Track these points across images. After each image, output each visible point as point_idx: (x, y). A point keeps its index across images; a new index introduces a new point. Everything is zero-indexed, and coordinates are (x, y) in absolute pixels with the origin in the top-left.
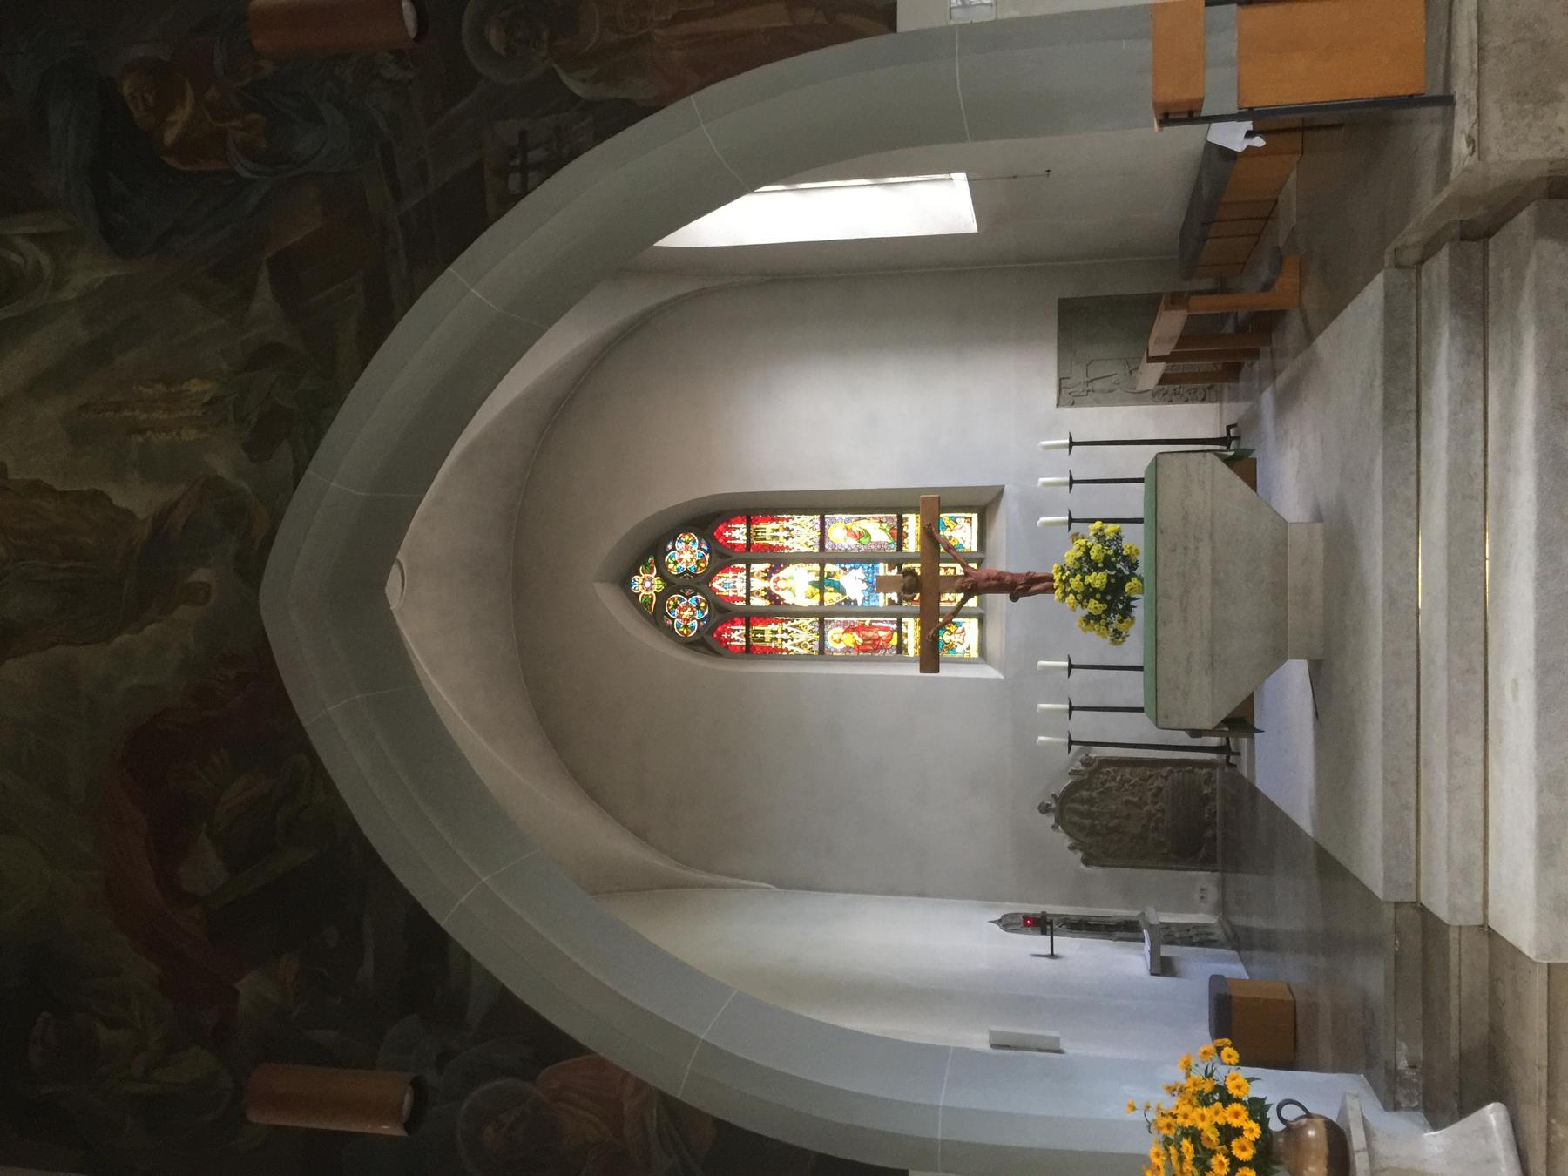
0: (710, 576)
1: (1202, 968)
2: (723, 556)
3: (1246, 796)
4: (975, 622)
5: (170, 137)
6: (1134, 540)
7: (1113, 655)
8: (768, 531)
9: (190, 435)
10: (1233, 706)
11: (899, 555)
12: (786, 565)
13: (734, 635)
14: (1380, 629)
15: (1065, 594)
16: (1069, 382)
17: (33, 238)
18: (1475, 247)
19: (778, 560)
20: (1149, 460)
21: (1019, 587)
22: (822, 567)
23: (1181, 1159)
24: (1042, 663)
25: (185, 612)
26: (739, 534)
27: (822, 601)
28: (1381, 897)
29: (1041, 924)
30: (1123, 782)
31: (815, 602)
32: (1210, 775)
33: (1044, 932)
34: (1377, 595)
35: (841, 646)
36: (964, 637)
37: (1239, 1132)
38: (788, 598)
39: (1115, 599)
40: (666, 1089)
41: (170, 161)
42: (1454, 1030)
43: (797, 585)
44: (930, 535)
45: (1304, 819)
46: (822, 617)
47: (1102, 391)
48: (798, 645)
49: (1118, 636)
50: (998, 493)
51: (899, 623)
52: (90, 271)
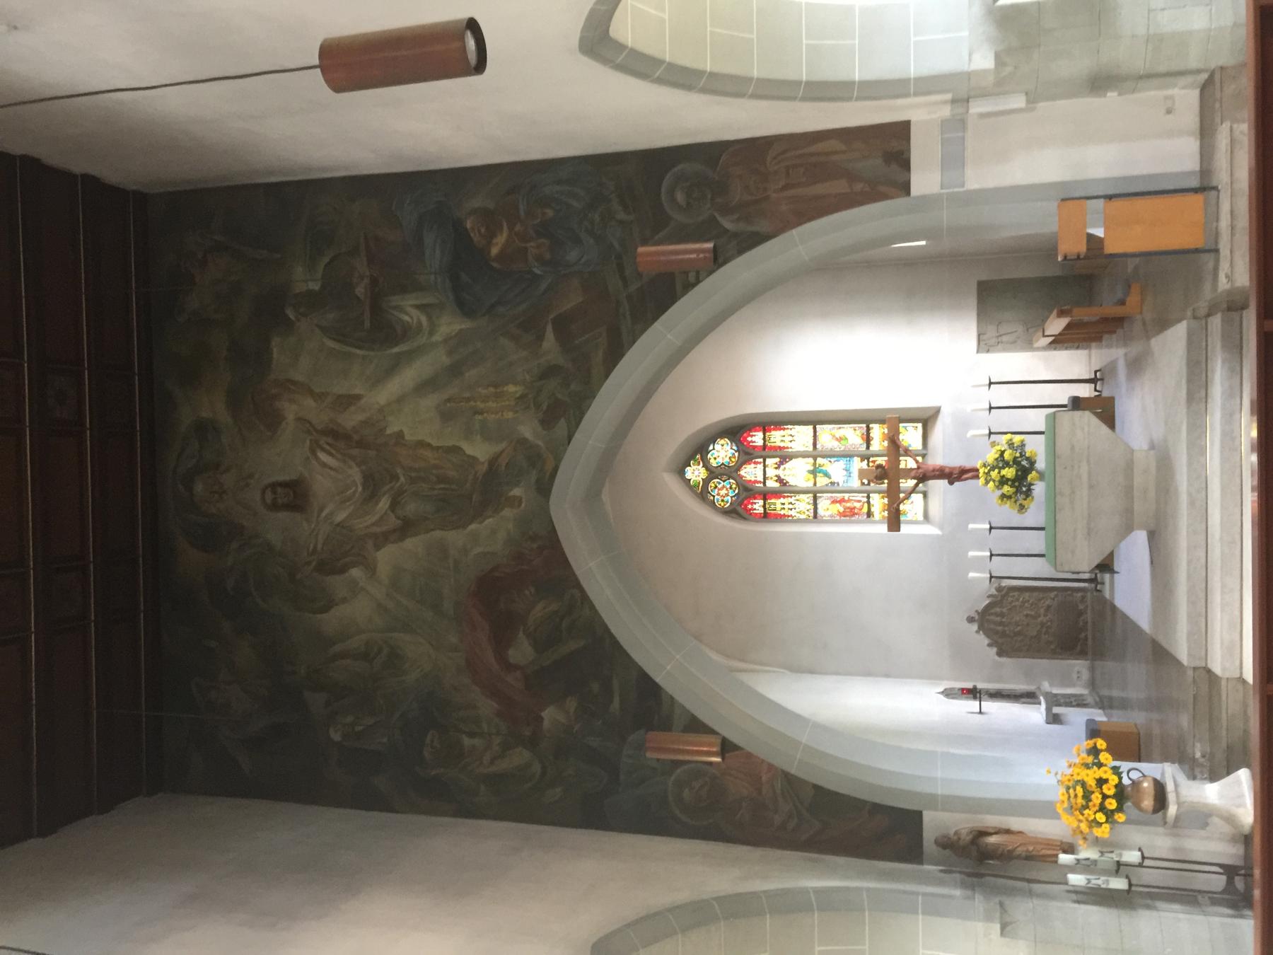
0: (739, 467)
1: (1078, 718)
2: (747, 453)
3: (1107, 611)
5: (495, 251)
6: (1036, 447)
7: (1017, 520)
8: (776, 437)
9: (510, 415)
10: (1102, 558)
11: (868, 452)
14: (1185, 518)
15: (987, 483)
17: (417, 307)
18: (1235, 315)
19: (785, 457)
20: (1047, 416)
21: (954, 475)
23: (1076, 796)
25: (507, 512)
28: (1185, 663)
29: (973, 693)
30: (1024, 602)
31: (810, 484)
32: (1083, 597)
33: (975, 698)
34: (1184, 499)
35: (829, 513)
36: (912, 508)
37: (1106, 781)
38: (792, 481)
39: (1021, 485)
40: (786, 768)
41: (495, 265)
42: (1224, 733)
45: (1144, 622)
49: (1022, 508)
50: (936, 412)
51: (868, 497)
52: (450, 325)
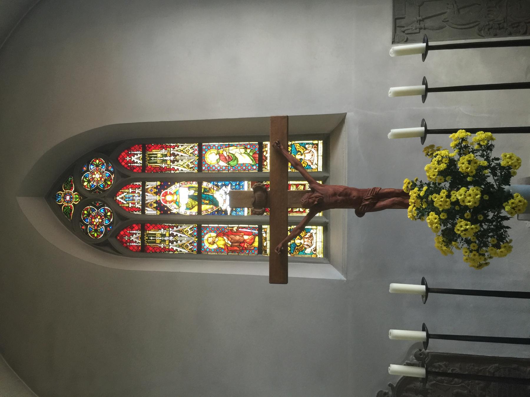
0: (115, 192)
2: (124, 176)
4: (320, 228)
11: (260, 175)
12: (173, 183)
13: (133, 238)
15: (422, 213)
16: (403, 22)
19: (167, 179)
21: (365, 202)
22: (200, 184)
24: (395, 286)
26: (137, 159)
27: (200, 211)
35: (215, 247)
43: (180, 198)
44: (281, 157)
46: (199, 224)
47: (433, 29)
48: (181, 246)
50: (340, 121)
